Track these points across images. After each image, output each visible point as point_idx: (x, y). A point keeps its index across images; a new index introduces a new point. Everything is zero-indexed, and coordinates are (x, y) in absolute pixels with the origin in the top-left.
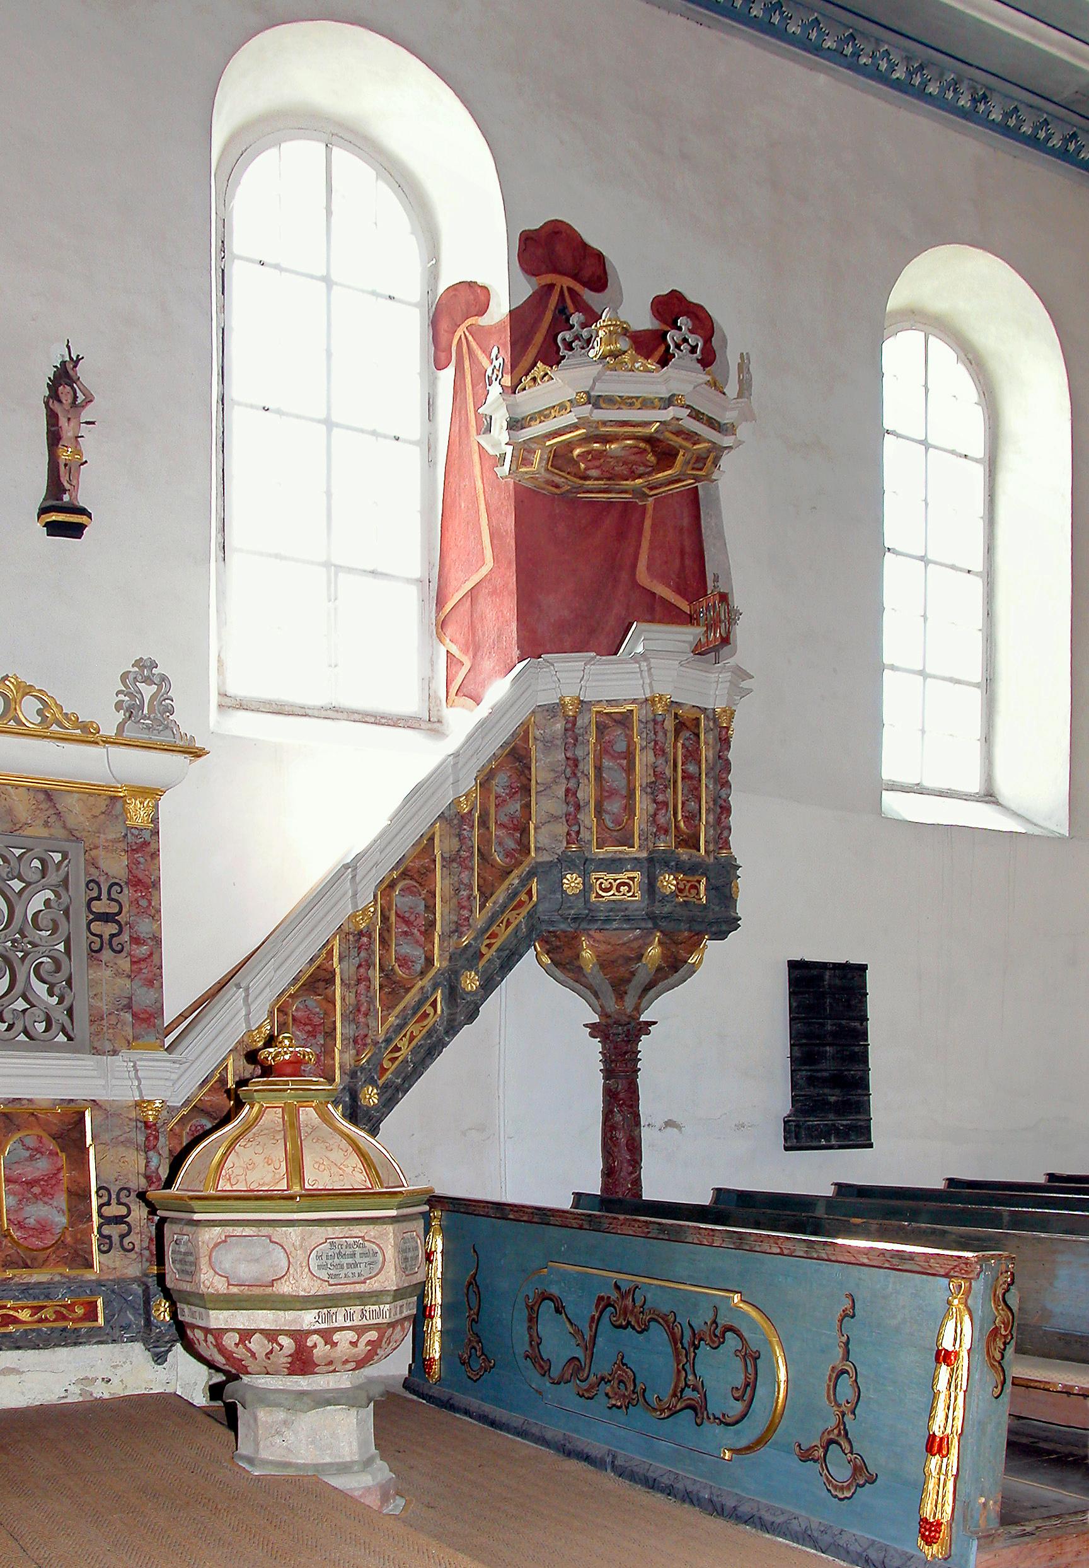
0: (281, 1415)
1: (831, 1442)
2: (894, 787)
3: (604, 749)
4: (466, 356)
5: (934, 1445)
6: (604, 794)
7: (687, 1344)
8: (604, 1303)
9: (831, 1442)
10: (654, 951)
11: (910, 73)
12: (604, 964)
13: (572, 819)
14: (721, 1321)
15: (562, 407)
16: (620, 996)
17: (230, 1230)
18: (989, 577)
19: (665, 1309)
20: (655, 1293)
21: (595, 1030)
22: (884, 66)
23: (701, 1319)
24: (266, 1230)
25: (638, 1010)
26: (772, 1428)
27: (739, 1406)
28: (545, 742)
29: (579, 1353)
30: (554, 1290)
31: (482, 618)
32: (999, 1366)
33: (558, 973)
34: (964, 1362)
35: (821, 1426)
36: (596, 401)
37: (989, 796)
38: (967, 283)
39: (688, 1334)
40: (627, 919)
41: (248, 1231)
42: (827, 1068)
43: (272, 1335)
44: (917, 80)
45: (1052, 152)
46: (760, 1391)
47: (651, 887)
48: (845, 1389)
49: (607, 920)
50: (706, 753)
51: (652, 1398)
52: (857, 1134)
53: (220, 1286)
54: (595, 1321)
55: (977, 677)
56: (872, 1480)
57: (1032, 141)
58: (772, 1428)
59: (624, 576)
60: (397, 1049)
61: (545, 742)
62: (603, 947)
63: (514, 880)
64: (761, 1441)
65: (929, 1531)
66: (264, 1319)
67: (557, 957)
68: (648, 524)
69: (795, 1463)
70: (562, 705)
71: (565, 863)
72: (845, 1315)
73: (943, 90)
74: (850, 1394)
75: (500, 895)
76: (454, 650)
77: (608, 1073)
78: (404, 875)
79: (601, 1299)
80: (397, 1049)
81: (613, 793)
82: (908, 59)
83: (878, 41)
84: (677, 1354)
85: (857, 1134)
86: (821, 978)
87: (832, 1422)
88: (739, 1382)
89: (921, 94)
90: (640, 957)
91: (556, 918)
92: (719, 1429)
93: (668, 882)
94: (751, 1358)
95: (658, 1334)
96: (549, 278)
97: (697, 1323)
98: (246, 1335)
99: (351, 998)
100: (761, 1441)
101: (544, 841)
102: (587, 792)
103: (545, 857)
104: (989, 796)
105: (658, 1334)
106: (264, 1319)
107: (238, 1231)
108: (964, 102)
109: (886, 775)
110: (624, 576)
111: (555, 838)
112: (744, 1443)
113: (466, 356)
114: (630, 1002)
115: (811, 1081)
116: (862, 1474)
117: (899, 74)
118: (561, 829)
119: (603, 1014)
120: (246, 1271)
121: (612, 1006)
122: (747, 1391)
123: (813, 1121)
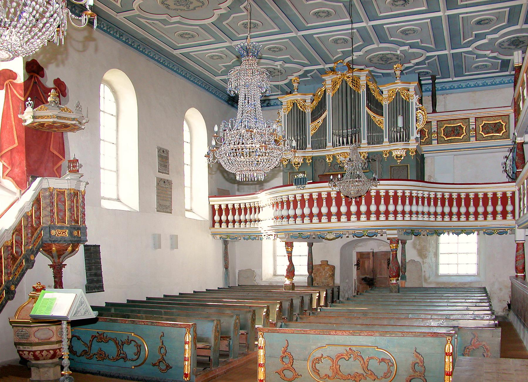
0: (46, 369)
1: (160, 361)
2: (105, 198)
3: (59, 200)
4: (9, 91)
5: (185, 359)
6: (59, 211)
7: (120, 345)
8: (94, 337)
9: (160, 361)
10: (70, 248)
11: (107, 29)
12: (58, 251)
13: (52, 217)
14: (130, 339)
15: (48, 116)
16: (59, 258)
17: (39, 328)
18: (117, 145)
19: (113, 337)
20: (109, 334)
21: (51, 266)
22: (102, 26)
23: (124, 339)
24: (48, 327)
25: (62, 262)
26: (145, 360)
27: (136, 357)
28: (44, 197)
29: (87, 349)
30: (77, 334)
31: (14, 157)
32: (195, 344)
33: (44, 252)
34: (190, 344)
35: (158, 359)
36: (58, 117)
37: (118, 200)
38: (118, 78)
39: (120, 343)
40: (65, 241)
41: (45, 327)
42: (93, 271)
43: (48, 351)
44: (109, 30)
45: (134, 48)
46: (142, 353)
47: (71, 234)
48: (163, 351)
49: (60, 241)
50: (80, 201)
51: (111, 357)
52: (101, 288)
53: (37, 341)
54: (91, 341)
55: (115, 170)
56: (171, 368)
57: (131, 45)
58: (145, 360)
59: (48, 149)
60: (16, 275)
61: (44, 197)
62: (58, 247)
63: (38, 231)
64: (143, 363)
65: (186, 376)
66: (47, 347)
67: (44, 249)
68: (53, 136)
69: (151, 367)
70: (49, 188)
71: (50, 228)
72: (161, 336)
73: (114, 33)
74: (164, 352)
75: (36, 235)
76: (5, 164)
77: (55, 277)
78: (16, 231)
79: (93, 336)
80: (16, 275)
81: (61, 211)
82: (107, 26)
83: (101, 21)
84: (118, 347)
85: (101, 288)
86: (91, 249)
87: (160, 358)
88: (136, 351)
89: (109, 33)
90: (66, 250)
91: (48, 240)
92: (131, 362)
93: (75, 233)
94: (139, 347)
95: (111, 343)
96: (32, 74)
97: (123, 340)
98: (42, 351)
99: (6, 263)
100: (143, 363)
101: (44, 221)
102: (55, 210)
103: (45, 225)
104: (118, 200)
105: (111, 343)
106: (47, 347)
107: (41, 328)
108: (118, 36)
109: (102, 195)
110: (48, 149)
111: (47, 221)
112: (138, 364)
113: (9, 91)
114: (61, 259)
115: (91, 275)
116: (168, 367)
117: (105, 29)
118: (49, 218)
119: (54, 262)
120: (43, 337)
121: (57, 261)
122: (138, 353)
123: (91, 285)
